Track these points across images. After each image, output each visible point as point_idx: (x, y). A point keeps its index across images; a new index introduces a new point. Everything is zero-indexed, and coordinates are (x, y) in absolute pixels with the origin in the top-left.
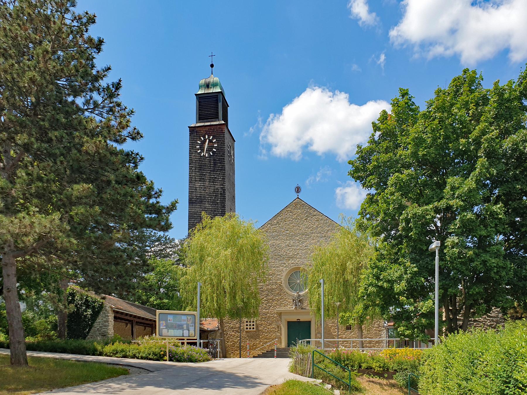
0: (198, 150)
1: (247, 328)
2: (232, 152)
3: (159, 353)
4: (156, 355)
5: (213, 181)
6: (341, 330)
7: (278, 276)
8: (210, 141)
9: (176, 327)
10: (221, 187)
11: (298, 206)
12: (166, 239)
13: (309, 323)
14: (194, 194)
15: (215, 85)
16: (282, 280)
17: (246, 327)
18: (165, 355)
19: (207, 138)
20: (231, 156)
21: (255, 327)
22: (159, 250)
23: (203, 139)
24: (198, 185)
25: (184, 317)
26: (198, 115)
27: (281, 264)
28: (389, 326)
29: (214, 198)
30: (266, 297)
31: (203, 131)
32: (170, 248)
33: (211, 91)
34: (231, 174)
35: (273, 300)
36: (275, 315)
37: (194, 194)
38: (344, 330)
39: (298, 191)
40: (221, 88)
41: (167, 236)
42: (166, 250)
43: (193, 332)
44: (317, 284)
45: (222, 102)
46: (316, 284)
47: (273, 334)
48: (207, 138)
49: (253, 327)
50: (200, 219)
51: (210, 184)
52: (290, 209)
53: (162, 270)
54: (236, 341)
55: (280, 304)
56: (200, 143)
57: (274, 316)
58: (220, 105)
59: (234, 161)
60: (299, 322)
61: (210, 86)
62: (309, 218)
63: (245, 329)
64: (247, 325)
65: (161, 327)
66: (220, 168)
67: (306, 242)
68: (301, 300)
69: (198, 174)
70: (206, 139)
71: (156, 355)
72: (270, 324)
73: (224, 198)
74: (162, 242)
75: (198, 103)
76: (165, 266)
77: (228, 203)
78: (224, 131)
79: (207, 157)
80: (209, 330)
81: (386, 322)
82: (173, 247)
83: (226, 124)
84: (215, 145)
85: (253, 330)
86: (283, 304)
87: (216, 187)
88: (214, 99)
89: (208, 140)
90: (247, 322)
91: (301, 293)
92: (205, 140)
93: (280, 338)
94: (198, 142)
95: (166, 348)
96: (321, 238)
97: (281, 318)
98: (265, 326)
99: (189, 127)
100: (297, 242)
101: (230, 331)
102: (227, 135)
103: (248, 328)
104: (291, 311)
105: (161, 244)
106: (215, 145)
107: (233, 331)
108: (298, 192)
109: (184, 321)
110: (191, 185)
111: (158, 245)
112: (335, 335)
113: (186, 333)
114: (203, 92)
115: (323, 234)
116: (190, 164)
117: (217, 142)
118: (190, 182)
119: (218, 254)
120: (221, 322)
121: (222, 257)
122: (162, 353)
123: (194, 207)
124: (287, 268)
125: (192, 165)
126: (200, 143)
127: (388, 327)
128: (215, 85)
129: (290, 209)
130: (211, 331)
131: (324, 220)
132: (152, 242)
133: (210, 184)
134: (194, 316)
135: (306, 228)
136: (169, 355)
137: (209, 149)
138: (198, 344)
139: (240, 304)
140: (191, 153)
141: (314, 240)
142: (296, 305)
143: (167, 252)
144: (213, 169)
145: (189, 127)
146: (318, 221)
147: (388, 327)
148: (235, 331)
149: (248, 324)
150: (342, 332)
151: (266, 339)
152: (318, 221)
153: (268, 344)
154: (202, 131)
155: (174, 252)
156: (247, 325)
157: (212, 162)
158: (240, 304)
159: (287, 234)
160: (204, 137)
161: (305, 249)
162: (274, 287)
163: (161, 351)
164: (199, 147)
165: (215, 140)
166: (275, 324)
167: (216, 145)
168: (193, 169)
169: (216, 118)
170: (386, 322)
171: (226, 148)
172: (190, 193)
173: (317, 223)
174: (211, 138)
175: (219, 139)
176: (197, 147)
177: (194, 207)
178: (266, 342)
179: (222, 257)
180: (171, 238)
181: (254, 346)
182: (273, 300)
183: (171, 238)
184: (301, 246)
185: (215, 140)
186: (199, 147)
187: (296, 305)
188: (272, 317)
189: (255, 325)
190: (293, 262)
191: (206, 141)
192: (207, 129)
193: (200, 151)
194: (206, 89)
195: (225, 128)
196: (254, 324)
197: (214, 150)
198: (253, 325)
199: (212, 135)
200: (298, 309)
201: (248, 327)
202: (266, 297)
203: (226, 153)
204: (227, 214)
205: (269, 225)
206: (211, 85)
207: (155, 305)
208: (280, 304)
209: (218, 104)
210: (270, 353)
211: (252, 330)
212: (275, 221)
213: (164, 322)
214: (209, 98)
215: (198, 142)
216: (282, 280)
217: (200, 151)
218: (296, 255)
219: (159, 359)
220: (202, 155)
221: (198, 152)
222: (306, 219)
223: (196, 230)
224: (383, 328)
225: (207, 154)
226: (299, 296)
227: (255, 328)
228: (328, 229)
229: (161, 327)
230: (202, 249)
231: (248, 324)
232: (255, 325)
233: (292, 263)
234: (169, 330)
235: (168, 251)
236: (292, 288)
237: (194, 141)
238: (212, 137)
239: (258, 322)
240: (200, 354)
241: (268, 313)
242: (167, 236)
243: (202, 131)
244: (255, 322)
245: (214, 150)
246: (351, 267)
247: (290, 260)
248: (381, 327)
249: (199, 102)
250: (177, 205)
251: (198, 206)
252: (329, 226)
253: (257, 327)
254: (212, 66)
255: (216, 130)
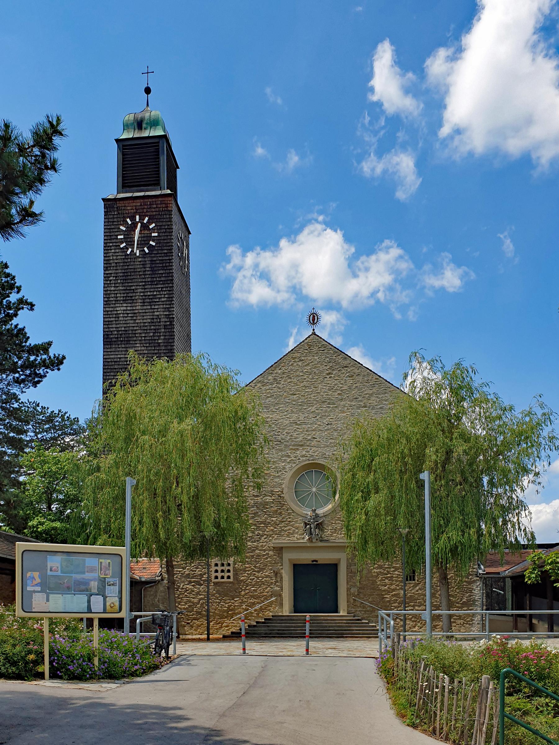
0: (122, 243)
1: (216, 577)
2: (185, 252)
3: (23, 658)
4: (14, 664)
5: (150, 301)
6: (396, 581)
7: (277, 480)
8: (145, 227)
9: (69, 588)
10: (165, 313)
11: (315, 349)
12: (63, 420)
13: (334, 568)
14: (114, 326)
15: (154, 123)
16: (283, 486)
17: (213, 575)
18: (40, 661)
19: (137, 220)
20: (184, 259)
21: (231, 575)
22: (51, 438)
23: (130, 222)
24: (121, 309)
25: (91, 562)
26: (121, 179)
27: (282, 456)
28: (487, 573)
29: (152, 334)
30: (253, 517)
31: (130, 208)
32: (70, 434)
33: (146, 134)
34: (184, 292)
35: (266, 524)
36: (271, 553)
37: (114, 326)
38: (401, 582)
39: (314, 317)
40: (164, 130)
41: (66, 413)
42: (63, 439)
43: (116, 600)
44: (362, 492)
45: (167, 155)
46: (360, 494)
47: (266, 588)
48: (137, 220)
49: (228, 574)
50: (125, 367)
51: (145, 307)
52: (299, 355)
53: (54, 468)
54: (196, 600)
55: (280, 531)
56: (124, 229)
57: (268, 554)
58: (163, 160)
59: (188, 269)
60: (314, 566)
61: (144, 125)
62: (334, 372)
63: (213, 577)
64: (216, 571)
65: (29, 588)
66: (163, 279)
67: (330, 416)
68: (321, 523)
69: (121, 288)
70: (137, 223)
71: (14, 664)
72: (261, 570)
73: (172, 336)
74: (57, 424)
75: (121, 156)
76: (59, 461)
77: (178, 344)
78: (170, 209)
79: (139, 257)
80: (143, 580)
81: (482, 567)
82: (76, 433)
83: (174, 196)
84: (153, 235)
85: (229, 580)
86: (286, 531)
87: (156, 314)
88: (152, 149)
89: (139, 224)
90: (216, 565)
91: (320, 512)
92: (134, 225)
93: (280, 595)
94: (122, 227)
95: (42, 644)
96: (358, 408)
97: (282, 558)
98: (251, 574)
99: (103, 200)
100: (311, 415)
101: (183, 582)
102: (175, 217)
103: (219, 577)
104: (304, 545)
105: (54, 429)
106: (153, 235)
107: (190, 582)
108: (314, 323)
109: (92, 570)
110: (107, 309)
111: (50, 429)
112: (384, 591)
113: (97, 603)
114: (131, 136)
115: (361, 401)
116: (106, 269)
117: (158, 228)
118: (107, 302)
119: (163, 432)
120: (170, 567)
121: (172, 437)
122: (32, 657)
123: (113, 350)
124: (294, 465)
125: (110, 272)
126: (124, 229)
127: (486, 576)
128: (154, 123)
129: (299, 355)
130: (146, 583)
131: (364, 376)
132: (39, 423)
133: (145, 307)
134: (118, 559)
135: (329, 390)
136: (51, 663)
137: (144, 241)
138: (127, 625)
139: (209, 531)
140: (107, 248)
141: (344, 412)
142: (311, 534)
143: (65, 441)
144: (149, 280)
145: (103, 200)
146: (352, 376)
147: (486, 576)
148: (194, 582)
149: (219, 568)
150: (398, 585)
151: (252, 597)
152: (352, 376)
153: (257, 607)
154: (129, 208)
155: (78, 442)
156: (216, 571)
157: (149, 266)
158: (209, 531)
159: (294, 401)
160: (133, 218)
161: (326, 430)
162: (268, 499)
163: (30, 652)
164: (122, 237)
165: (154, 225)
166: (271, 569)
167: (156, 234)
168: (111, 278)
169: (156, 184)
170: (482, 567)
171: (175, 241)
172: (106, 323)
173: (350, 381)
174: (145, 221)
175: (161, 224)
176: (119, 237)
177: (113, 350)
178: (254, 604)
179: (172, 437)
180: (72, 417)
181: (229, 609)
182: (266, 524)
183: (72, 417)
184: (319, 423)
185: (154, 225)
186: (122, 237)
187: (311, 534)
188: (264, 555)
189: (232, 571)
190: (304, 453)
191: (136, 227)
192: (138, 203)
193: (124, 244)
194: (136, 131)
195: (173, 202)
196: (231, 568)
197: (151, 243)
198: (229, 571)
199: (147, 216)
200: (314, 540)
201: (219, 575)
202: (253, 517)
203: (175, 251)
204: (179, 355)
205: (259, 385)
206: (147, 124)
207: (41, 533)
208: (280, 531)
209: (159, 158)
210: (264, 626)
211: (226, 580)
212: (270, 378)
213: (36, 574)
214: (143, 148)
215: (122, 227)
216: (283, 486)
217: (124, 244)
218: (310, 440)
219: (23, 673)
220: (128, 252)
221: (122, 246)
222: (328, 374)
223: (118, 385)
224: (475, 578)
225: (138, 251)
226: (317, 516)
227: (232, 577)
228: (371, 392)
229: (29, 588)
230: (131, 418)
231: (219, 568)
232: (232, 571)
233: (303, 456)
234: (51, 596)
235: (67, 440)
236: (302, 501)
237: (113, 227)
238: (147, 219)
239: (239, 565)
240: (133, 655)
241: (257, 548)
242: (66, 413)
243: (129, 208)
244: (232, 565)
245: (151, 243)
246: (434, 457)
247: (298, 449)
248: (471, 575)
249: (123, 155)
250: (56, 140)
251: (121, 349)
252: (373, 386)
253: (236, 575)
254: (148, 91)
255: (155, 206)
